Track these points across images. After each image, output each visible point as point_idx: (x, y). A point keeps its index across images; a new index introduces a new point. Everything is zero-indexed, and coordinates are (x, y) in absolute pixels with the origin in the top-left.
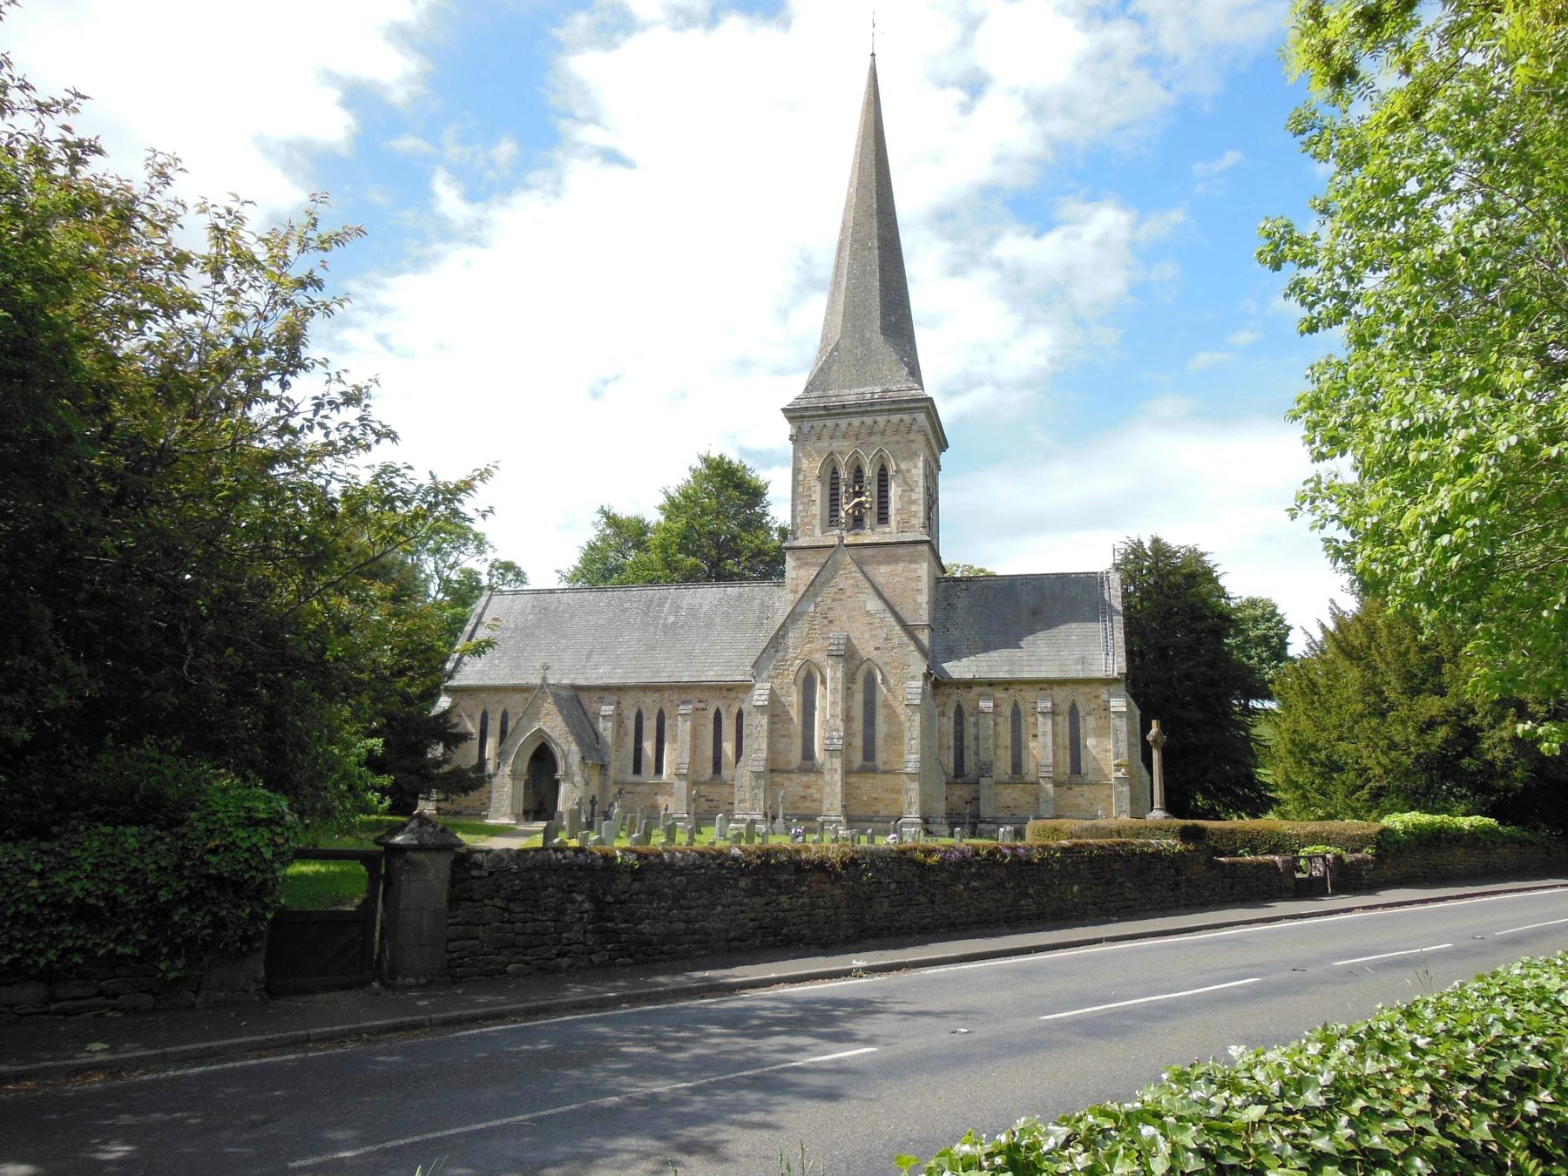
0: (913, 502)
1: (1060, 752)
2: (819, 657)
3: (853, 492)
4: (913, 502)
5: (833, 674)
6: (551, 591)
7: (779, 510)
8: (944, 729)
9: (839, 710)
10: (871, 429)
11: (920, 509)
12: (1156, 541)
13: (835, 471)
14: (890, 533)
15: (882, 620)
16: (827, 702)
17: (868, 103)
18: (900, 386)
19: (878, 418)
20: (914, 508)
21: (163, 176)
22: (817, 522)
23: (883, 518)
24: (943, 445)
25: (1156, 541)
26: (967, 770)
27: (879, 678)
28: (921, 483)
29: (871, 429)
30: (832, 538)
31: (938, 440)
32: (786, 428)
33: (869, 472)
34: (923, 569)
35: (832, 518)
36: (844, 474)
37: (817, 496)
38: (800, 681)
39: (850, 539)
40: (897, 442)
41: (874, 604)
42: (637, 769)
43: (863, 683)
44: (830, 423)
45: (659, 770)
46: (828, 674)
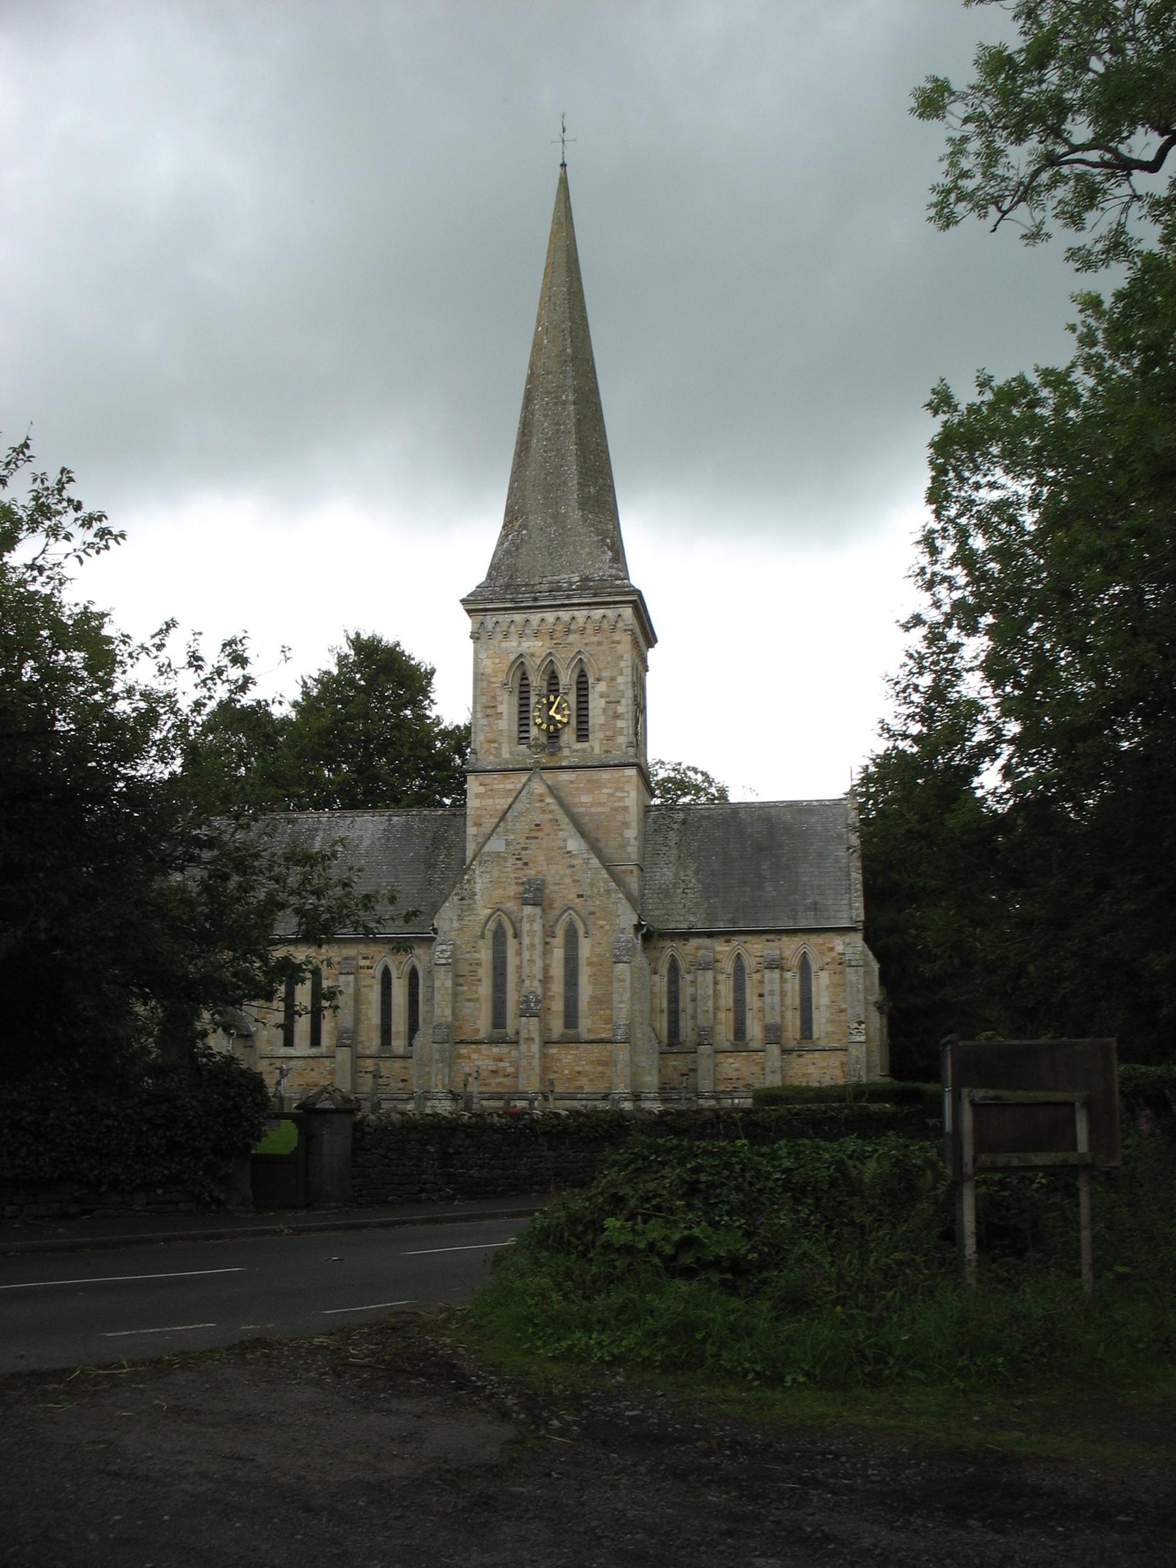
0: (617, 716)
4: (617, 716)
7: (451, 704)
13: (524, 677)
15: (587, 861)
19: (576, 614)
20: (620, 724)
23: (582, 734)
32: (466, 623)
33: (566, 678)
38: (489, 935)
40: (600, 644)
41: (575, 844)
42: (413, 975)
44: (518, 617)
45: (315, 1040)
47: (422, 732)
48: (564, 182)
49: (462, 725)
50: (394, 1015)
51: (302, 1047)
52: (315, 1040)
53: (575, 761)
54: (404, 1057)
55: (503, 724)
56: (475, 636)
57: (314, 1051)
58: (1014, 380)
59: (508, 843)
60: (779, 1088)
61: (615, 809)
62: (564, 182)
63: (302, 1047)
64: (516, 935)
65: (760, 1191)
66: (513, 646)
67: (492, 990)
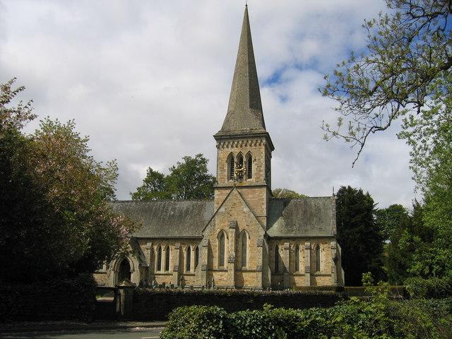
0: (261, 171)
1: (313, 264)
2: (226, 228)
3: (238, 166)
4: (261, 171)
5: (231, 234)
6: (128, 202)
7: (212, 169)
8: (272, 255)
9: (233, 248)
10: (246, 135)
11: (263, 173)
12: (349, 187)
13: (233, 159)
14: (252, 181)
16: (229, 245)
17: (244, 23)
18: (254, 125)
21: (325, 138)
22: (226, 178)
23: (250, 177)
24: (273, 149)
25: (349, 187)
26: (279, 270)
27: (248, 236)
28: (264, 164)
29: (246, 135)
30: (231, 182)
31: (270, 147)
32: (215, 143)
34: (263, 194)
35: (231, 177)
36: (236, 160)
37: (226, 168)
39: (238, 184)
41: (246, 209)
43: (240, 237)
45: (167, 268)
46: (230, 235)
47: (204, 178)
48: (247, 10)
49: (381, 203)
50: (162, 258)
51: (162, 271)
52: (167, 268)
53: (247, 184)
54: (194, 275)
55: (226, 173)
56: (218, 147)
57: (166, 272)
58: (301, 36)
59: (226, 209)
60: (307, 288)
61: (260, 199)
62: (247, 10)
63: (162, 271)
64: (227, 238)
65: (334, 323)
66: (230, 150)
67: (225, 253)
